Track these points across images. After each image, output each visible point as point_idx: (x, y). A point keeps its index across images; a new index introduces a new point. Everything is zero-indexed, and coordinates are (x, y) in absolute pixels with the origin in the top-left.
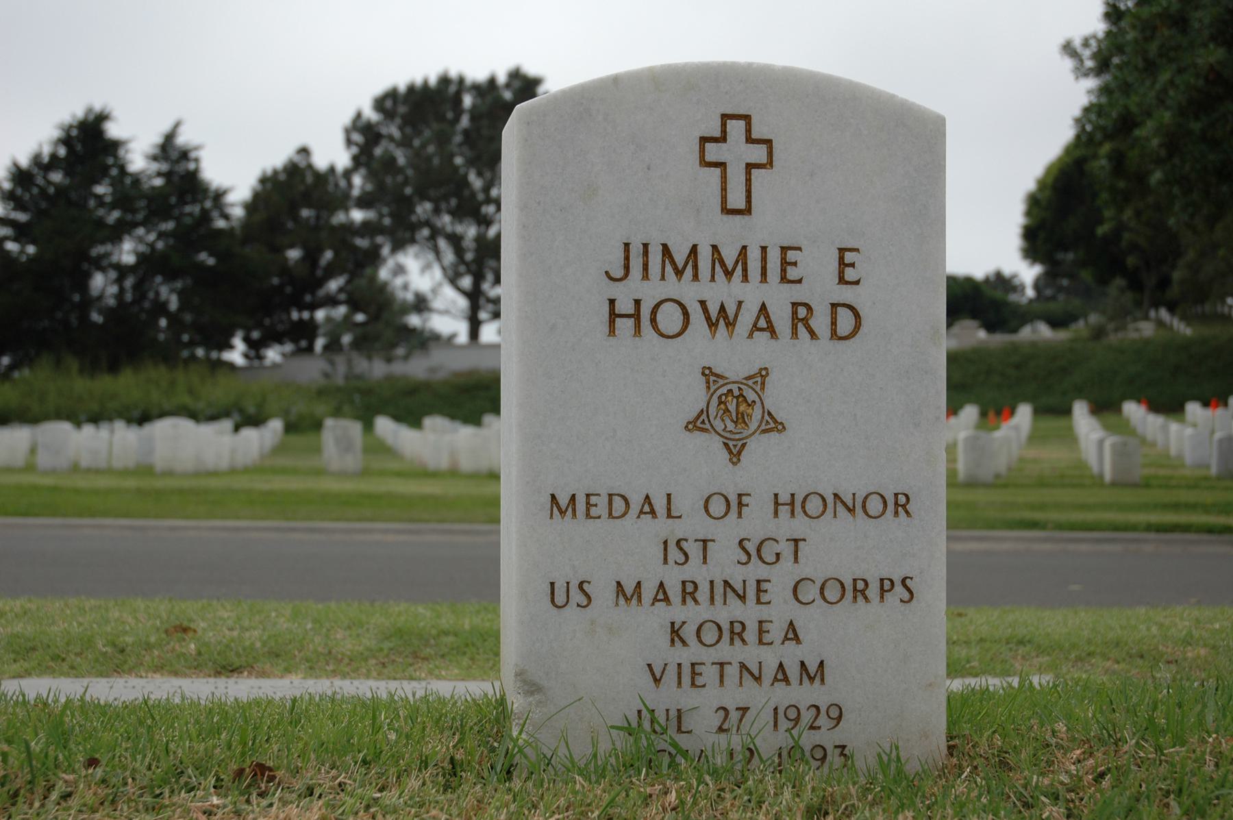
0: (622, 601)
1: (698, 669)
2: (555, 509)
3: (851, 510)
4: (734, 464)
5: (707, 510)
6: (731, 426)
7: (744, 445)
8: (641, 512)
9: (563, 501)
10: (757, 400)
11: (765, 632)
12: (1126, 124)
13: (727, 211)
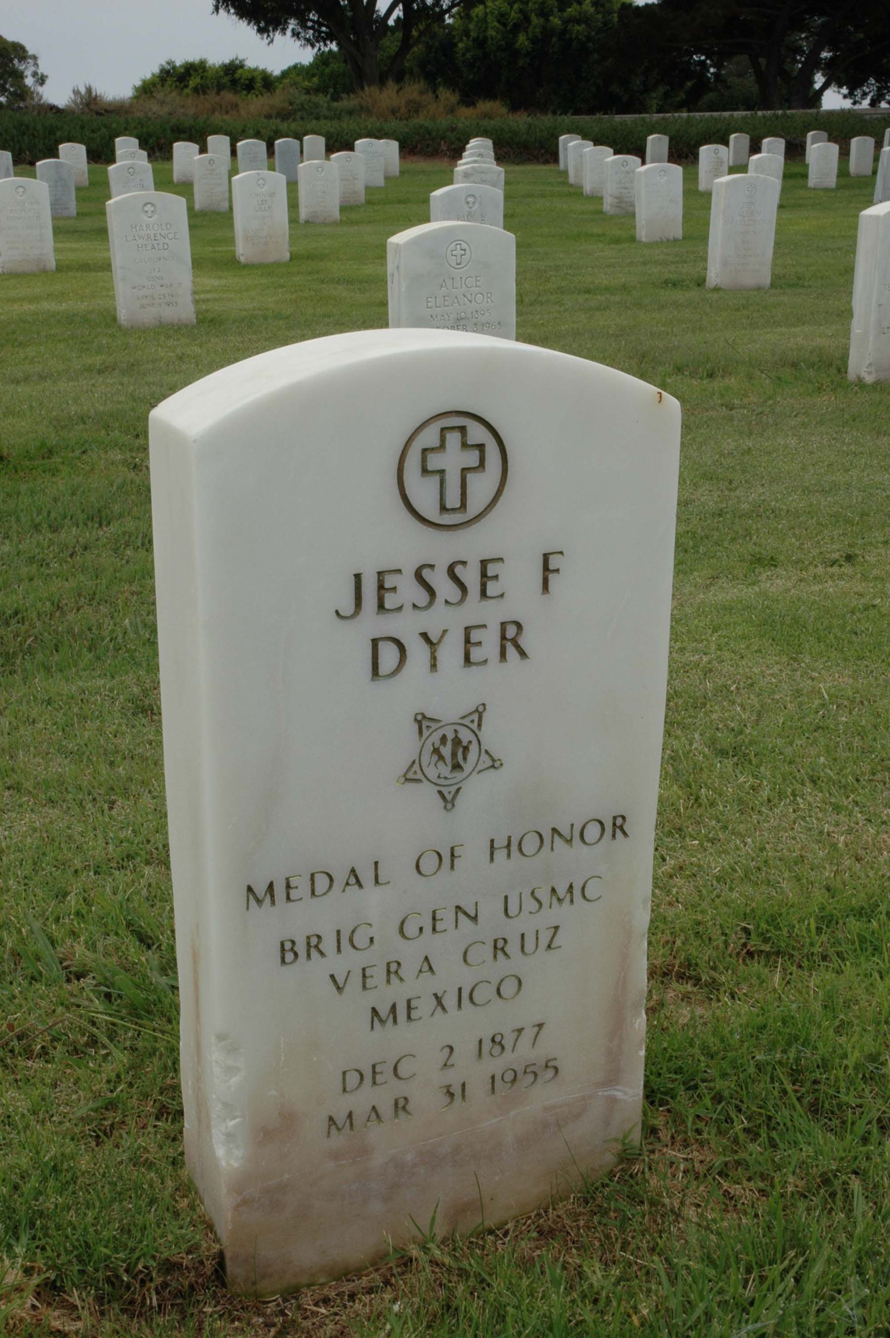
5: (419, 871)
7: (458, 790)
9: (260, 889)
10: (475, 742)
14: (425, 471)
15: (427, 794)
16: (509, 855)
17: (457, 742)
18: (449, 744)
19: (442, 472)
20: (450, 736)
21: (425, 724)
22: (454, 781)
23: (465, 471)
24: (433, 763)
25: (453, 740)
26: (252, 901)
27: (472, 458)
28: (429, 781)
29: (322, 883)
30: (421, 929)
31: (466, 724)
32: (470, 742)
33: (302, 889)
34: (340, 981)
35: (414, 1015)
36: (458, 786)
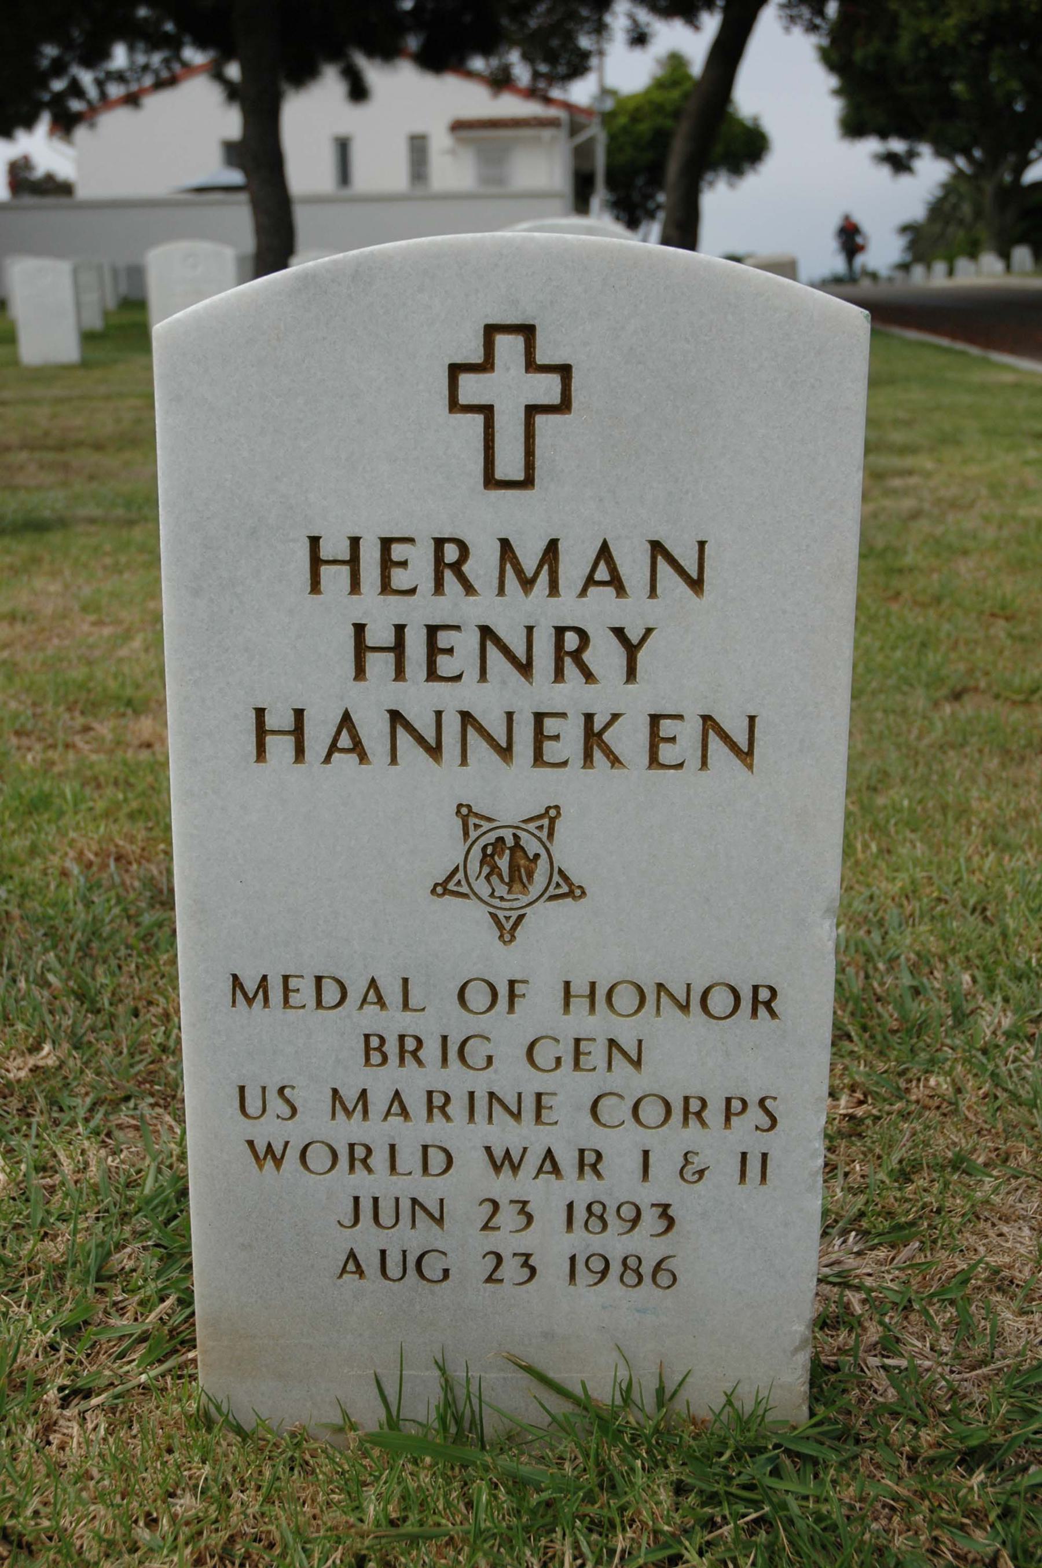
0: (340, 1114)
2: (238, 992)
3: (685, 1008)
4: (433, 891)
6: (501, 890)
10: (544, 855)
11: (519, 996)
12: (867, 651)
13: (491, 481)
19: (487, 411)
20: (510, 842)
21: (472, 821)
22: (516, 904)
29: (331, 994)
30: (558, 1060)
32: (537, 856)
36: (556, 870)
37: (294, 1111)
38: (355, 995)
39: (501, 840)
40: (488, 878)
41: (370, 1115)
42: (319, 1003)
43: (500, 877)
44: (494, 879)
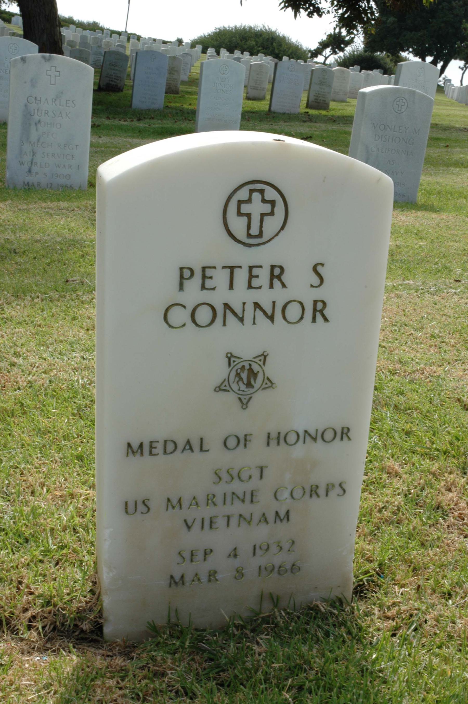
1: (209, 273)
3: (315, 439)
4: (215, 390)
6: (243, 387)
8: (184, 449)
9: (175, 502)
14: (239, 214)
15: (231, 398)
16: (278, 443)
17: (251, 370)
18: (246, 372)
19: (249, 216)
20: (247, 367)
21: (232, 359)
23: (263, 215)
24: (236, 381)
25: (248, 370)
26: (170, 507)
27: (267, 208)
28: (234, 391)
29: (170, 447)
31: (256, 361)
33: (159, 448)
34: (190, 523)
35: (214, 526)
36: (266, 378)
37: (149, 509)
38: (180, 447)
39: (243, 366)
40: (237, 382)
41: (182, 506)
42: (165, 452)
43: (243, 382)
44: (240, 383)
